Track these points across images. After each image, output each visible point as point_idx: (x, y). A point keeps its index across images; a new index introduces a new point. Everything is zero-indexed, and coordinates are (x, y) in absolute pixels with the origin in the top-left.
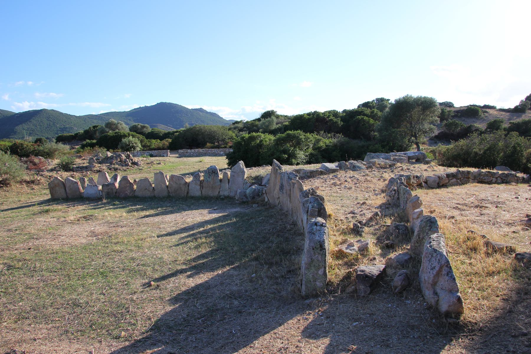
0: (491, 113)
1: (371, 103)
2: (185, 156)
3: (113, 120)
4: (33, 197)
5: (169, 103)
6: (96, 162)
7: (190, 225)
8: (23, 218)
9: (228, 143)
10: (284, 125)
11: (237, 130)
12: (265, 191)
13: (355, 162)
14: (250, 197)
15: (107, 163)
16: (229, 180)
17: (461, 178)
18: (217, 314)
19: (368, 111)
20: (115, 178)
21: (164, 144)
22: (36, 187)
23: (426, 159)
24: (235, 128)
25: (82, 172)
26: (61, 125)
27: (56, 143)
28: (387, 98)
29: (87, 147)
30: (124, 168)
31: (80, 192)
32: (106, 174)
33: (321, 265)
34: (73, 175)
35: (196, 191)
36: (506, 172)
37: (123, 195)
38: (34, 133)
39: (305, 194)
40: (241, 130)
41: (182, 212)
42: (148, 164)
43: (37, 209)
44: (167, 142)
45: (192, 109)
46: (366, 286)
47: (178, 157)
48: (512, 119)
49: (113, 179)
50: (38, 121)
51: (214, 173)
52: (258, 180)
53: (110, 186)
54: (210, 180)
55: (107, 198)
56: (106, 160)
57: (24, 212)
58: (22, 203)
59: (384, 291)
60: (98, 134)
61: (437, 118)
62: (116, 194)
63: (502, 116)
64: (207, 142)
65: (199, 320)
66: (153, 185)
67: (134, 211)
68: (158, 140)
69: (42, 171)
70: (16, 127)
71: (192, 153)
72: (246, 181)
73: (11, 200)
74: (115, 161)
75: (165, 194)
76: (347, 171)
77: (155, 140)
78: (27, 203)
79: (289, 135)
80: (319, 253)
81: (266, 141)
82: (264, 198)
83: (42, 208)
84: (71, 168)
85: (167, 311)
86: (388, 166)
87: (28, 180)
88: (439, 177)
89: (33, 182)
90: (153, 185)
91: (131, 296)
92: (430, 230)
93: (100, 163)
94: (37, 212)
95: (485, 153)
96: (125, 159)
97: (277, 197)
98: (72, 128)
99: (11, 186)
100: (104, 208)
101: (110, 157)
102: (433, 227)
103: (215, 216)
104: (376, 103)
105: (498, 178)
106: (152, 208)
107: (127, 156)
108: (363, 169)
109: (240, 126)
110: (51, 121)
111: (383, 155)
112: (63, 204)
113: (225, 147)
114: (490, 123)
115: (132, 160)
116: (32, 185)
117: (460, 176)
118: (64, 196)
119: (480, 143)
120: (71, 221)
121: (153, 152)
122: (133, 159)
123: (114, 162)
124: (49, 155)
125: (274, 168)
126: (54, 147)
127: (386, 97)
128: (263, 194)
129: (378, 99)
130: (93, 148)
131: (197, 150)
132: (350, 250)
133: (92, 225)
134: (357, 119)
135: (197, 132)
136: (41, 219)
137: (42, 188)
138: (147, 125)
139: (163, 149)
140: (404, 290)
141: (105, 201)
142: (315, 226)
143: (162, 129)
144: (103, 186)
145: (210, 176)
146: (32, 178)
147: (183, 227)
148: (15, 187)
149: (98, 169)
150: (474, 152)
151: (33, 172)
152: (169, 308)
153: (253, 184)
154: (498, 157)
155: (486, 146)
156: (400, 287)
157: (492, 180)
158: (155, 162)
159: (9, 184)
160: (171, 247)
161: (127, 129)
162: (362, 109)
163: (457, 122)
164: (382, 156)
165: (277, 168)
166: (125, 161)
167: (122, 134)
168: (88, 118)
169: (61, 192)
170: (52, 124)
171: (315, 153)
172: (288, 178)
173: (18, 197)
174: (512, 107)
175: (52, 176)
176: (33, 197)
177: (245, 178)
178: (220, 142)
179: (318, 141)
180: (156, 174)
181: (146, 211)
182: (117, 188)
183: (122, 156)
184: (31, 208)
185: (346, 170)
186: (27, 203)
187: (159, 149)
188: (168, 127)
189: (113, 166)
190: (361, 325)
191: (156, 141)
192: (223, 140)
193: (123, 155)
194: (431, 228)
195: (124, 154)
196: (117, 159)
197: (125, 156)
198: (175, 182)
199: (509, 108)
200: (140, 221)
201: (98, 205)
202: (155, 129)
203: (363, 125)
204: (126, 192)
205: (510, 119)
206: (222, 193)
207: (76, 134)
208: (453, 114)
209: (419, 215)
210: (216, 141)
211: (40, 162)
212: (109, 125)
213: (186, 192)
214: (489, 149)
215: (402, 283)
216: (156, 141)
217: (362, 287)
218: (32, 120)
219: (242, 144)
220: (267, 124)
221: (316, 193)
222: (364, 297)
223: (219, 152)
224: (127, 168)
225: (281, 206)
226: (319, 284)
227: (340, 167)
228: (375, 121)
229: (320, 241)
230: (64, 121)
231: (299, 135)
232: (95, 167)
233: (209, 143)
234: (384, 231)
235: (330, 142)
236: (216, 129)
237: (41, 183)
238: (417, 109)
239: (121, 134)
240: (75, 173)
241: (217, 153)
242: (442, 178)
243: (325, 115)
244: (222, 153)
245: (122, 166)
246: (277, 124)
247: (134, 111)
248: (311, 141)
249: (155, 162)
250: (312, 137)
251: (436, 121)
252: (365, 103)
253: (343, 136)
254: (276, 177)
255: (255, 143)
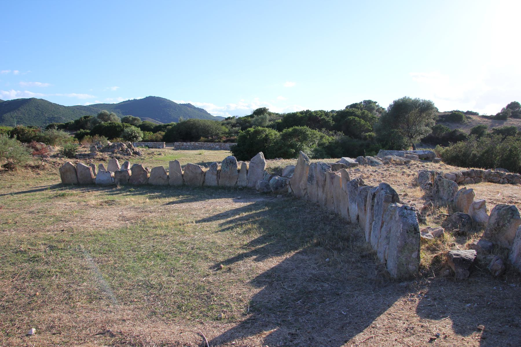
0: (474, 119)
1: (359, 105)
2: (181, 149)
3: (106, 111)
4: (41, 181)
5: (158, 98)
6: (98, 150)
7: (222, 212)
8: (40, 201)
9: (222, 137)
10: (277, 122)
11: (230, 126)
12: (289, 182)
13: (372, 158)
14: (273, 187)
15: (109, 152)
16: (247, 171)
17: (474, 177)
18: (313, 295)
19: (359, 112)
20: (126, 165)
21: (157, 137)
22: (42, 172)
23: (435, 158)
24: (228, 124)
25: (85, 160)
26: (50, 115)
27: (57, 129)
28: (374, 101)
29: (87, 135)
30: (126, 157)
31: (91, 178)
32: (116, 161)
33: (415, 249)
34: (77, 162)
35: (212, 180)
36: (512, 174)
37: (136, 182)
38: (22, 121)
39: (353, 183)
40: (234, 126)
41: (206, 200)
42: (148, 154)
43: (51, 193)
44: (161, 134)
45: (180, 104)
46: (465, 270)
47: (173, 150)
48: (493, 126)
49: (124, 166)
50: (27, 109)
51: (232, 163)
52: (278, 171)
53: (123, 173)
54: (227, 170)
55: (121, 184)
56: (107, 149)
57: (38, 195)
58: (31, 187)
59: (482, 274)
60: (89, 124)
61: (432, 121)
62: (129, 181)
63: (484, 123)
64: (201, 136)
65: (297, 302)
66: (168, 174)
67: (156, 198)
68: (151, 132)
69: (45, 157)
70: (4, 115)
71: (188, 146)
72: (266, 172)
73: (18, 184)
74: (117, 150)
75: (180, 182)
76: (366, 166)
77: (148, 132)
78: (37, 187)
79: (295, 131)
80: (413, 237)
81: (271, 135)
82: (288, 189)
83: (55, 192)
84: (74, 155)
85: (255, 293)
86: (403, 163)
87: (33, 165)
88: (456, 175)
89: (38, 167)
90: (168, 174)
91: (205, 278)
92: (512, 218)
93: (102, 151)
94: (52, 196)
95: (483, 155)
96: (126, 149)
97: (304, 188)
98: (60, 118)
99: (17, 170)
100: (121, 194)
101: (111, 146)
102: (515, 215)
103: (242, 204)
104: (363, 105)
105: (505, 179)
106: (173, 196)
107: (128, 146)
108: (381, 165)
109: (233, 121)
110: (39, 110)
111: (396, 152)
112: (76, 189)
113: (219, 142)
114: (473, 129)
115: (133, 150)
116: (37, 170)
117: (474, 175)
118: (76, 181)
119: (478, 147)
120: (94, 205)
121: (149, 144)
122: (135, 149)
123: (116, 151)
124: (50, 141)
125: (301, 159)
126: (55, 134)
127: (374, 100)
128: (286, 185)
129: (366, 101)
130: (93, 137)
131: (193, 143)
132: (427, 236)
133: (118, 210)
134: (348, 119)
135: (191, 126)
136: (60, 203)
137: (47, 174)
138: (138, 118)
139: (156, 141)
140: (504, 274)
141: (119, 187)
142: (406, 210)
143: (153, 122)
144: (116, 173)
145: (228, 166)
146: (37, 164)
147: (215, 213)
148: (20, 171)
149: (101, 157)
150: (473, 153)
151: (36, 157)
152: (257, 290)
153: (273, 175)
154: (495, 159)
155: (485, 148)
156: (500, 271)
157: (500, 180)
158: (155, 153)
159: (13, 168)
160: (217, 232)
161: (119, 121)
162: (353, 110)
163: (442, 126)
164: (395, 154)
165: (305, 159)
166: (127, 151)
167: (117, 125)
168: (77, 108)
169: (71, 177)
170: (40, 113)
171: (320, 149)
172: (321, 168)
173: (25, 181)
174: (494, 114)
175: (56, 162)
176: (41, 181)
177: (265, 169)
178: (214, 136)
179: (322, 137)
180: (171, 163)
181: (168, 198)
182: (130, 175)
183: (124, 146)
184: (44, 192)
185: (365, 165)
186: (37, 187)
187: (152, 141)
188: (156, 121)
189: (115, 155)
190: (474, 306)
191: (149, 133)
192: (217, 135)
193: (124, 144)
194: (514, 215)
195: (125, 144)
196: (118, 149)
197: (126, 145)
198: (191, 171)
199: (492, 115)
200: (167, 207)
201: (113, 191)
202: (146, 122)
203: (354, 125)
204: (140, 180)
205: (492, 126)
206: (239, 184)
207: (67, 124)
208: (438, 119)
209: (482, 205)
210: (210, 135)
211: (43, 149)
212: (102, 116)
213: (202, 181)
214: (487, 152)
215: (502, 267)
216: (149, 133)
217: (460, 270)
218: (20, 108)
219: (247, 138)
220: (260, 120)
221: (363, 183)
222: (463, 279)
223: (215, 146)
224: (129, 158)
225: (308, 196)
226: (411, 267)
227: (360, 162)
228: (366, 122)
229: (414, 225)
230: (52, 111)
231: (306, 130)
232: (97, 155)
233: (203, 137)
234: (446, 220)
235: (333, 139)
236: (209, 124)
237: (46, 168)
238: (415, 111)
239: (115, 124)
240: (79, 160)
241: (212, 147)
242: (459, 176)
243: (317, 114)
244: (217, 147)
245: (124, 155)
246: (270, 121)
247: (123, 103)
248: (317, 137)
249: (155, 153)
250: (318, 133)
251: (431, 123)
252: (353, 104)
253: (343, 134)
254: (303, 169)
255: (261, 137)
